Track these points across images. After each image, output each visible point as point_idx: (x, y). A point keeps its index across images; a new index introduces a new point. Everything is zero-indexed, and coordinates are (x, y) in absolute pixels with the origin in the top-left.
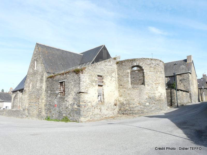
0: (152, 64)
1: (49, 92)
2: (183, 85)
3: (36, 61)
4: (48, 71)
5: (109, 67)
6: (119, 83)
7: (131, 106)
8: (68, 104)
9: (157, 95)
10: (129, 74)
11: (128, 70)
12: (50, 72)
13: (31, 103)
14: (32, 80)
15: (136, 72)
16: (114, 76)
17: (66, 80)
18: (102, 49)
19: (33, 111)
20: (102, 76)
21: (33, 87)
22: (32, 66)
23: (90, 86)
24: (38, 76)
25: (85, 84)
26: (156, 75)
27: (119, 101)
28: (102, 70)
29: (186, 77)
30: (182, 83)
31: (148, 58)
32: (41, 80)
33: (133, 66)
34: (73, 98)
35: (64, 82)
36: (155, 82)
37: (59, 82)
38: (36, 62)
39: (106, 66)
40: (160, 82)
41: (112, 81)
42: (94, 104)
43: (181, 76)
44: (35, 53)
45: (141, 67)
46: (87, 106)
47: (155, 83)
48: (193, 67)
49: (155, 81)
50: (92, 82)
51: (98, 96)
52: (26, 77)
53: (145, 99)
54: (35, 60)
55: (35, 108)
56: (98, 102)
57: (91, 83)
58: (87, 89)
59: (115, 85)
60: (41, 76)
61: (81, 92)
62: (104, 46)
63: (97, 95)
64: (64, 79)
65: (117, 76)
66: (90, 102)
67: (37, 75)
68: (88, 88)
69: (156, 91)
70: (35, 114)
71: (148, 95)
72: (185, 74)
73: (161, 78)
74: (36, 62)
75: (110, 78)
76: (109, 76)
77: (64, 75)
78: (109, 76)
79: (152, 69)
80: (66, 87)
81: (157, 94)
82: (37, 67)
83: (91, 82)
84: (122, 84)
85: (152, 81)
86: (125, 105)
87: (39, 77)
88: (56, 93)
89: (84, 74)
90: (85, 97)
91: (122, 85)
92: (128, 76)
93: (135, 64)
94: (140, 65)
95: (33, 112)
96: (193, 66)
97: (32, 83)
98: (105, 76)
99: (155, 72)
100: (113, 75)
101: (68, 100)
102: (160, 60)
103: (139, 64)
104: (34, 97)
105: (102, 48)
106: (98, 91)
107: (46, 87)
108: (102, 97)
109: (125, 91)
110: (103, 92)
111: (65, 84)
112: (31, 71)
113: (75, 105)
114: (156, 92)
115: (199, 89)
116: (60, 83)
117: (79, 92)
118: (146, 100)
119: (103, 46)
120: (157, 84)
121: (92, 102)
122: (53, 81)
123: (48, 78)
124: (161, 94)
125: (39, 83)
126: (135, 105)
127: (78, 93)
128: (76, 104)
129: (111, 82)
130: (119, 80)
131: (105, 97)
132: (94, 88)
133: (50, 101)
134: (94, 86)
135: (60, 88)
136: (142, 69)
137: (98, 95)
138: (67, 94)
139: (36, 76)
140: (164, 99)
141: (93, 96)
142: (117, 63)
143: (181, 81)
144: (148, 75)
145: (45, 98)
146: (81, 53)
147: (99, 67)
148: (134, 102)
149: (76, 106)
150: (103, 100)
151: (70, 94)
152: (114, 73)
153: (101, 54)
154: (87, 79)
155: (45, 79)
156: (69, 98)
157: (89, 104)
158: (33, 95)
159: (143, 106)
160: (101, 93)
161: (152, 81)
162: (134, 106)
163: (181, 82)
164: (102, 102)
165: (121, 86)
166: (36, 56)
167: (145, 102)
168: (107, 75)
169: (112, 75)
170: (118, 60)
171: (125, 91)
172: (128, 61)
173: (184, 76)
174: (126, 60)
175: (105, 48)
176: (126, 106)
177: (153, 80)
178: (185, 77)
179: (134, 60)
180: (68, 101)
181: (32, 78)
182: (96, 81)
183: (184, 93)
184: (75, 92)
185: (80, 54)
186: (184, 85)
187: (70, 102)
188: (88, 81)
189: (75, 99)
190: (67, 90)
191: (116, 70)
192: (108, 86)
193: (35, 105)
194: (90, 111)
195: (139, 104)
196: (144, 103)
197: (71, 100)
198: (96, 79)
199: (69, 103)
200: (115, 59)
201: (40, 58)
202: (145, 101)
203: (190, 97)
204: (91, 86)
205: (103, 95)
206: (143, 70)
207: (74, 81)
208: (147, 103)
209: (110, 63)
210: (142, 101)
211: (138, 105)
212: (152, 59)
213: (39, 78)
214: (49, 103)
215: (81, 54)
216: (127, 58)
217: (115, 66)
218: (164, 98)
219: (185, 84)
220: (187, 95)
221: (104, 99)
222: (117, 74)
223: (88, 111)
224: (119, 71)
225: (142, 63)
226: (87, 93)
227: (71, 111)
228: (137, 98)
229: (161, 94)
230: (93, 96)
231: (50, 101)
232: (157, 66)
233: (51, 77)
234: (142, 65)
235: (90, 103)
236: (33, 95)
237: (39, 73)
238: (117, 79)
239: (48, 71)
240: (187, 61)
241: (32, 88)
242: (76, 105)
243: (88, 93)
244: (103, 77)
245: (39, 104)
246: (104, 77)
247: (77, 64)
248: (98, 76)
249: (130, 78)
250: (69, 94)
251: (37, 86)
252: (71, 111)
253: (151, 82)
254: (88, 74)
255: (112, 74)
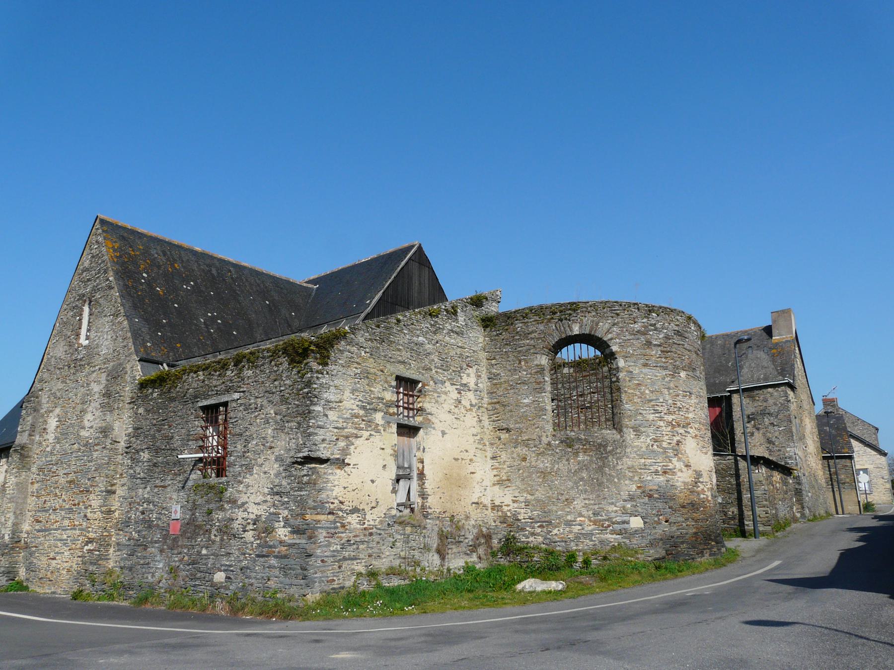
0: (656, 329)
1: (145, 456)
2: (763, 440)
3: (89, 304)
4: (148, 354)
5: (447, 338)
6: (494, 418)
7: (555, 531)
8: (240, 521)
9: (682, 478)
10: (547, 373)
11: (538, 356)
12: (154, 355)
13: (47, 511)
14: (58, 394)
15: (566, 370)
16: (472, 385)
17: (236, 396)
18: (407, 263)
19: (52, 555)
20: (416, 382)
21: (63, 434)
22: (66, 328)
23: (356, 428)
24: (94, 375)
25: (333, 416)
26: (672, 385)
27: (493, 509)
28: (416, 349)
29: (775, 404)
30: (758, 429)
31: (635, 304)
32: (107, 394)
33: (564, 336)
34: (266, 491)
35: (225, 404)
36: (670, 418)
37: (200, 404)
38: (86, 309)
39: (435, 333)
40: (691, 416)
41: (463, 410)
42: (373, 518)
43: (753, 398)
44: (87, 264)
45: (605, 342)
46: (341, 530)
47: (670, 423)
48: (799, 361)
49: (670, 413)
50: (369, 408)
51: (398, 481)
52: (20, 406)
53: (625, 501)
54: (81, 298)
55: (65, 537)
56: (394, 512)
57: (362, 412)
58: (342, 444)
59: (477, 430)
60: (108, 375)
61: (313, 455)
62: (420, 248)
63: (392, 472)
64: (228, 390)
65: (484, 384)
66: (355, 510)
67: (87, 369)
68: (347, 437)
69: (674, 460)
70: (64, 572)
71: (636, 478)
72: (770, 390)
73: (693, 397)
74: (86, 309)
75: (455, 395)
76: (448, 384)
77: (229, 373)
78: (448, 384)
79: (655, 352)
80: (237, 430)
81: (679, 474)
82: (88, 330)
83: (364, 408)
84: (512, 426)
85: (656, 412)
86: (523, 529)
87: (99, 382)
88: (179, 462)
89: (334, 367)
90: (338, 485)
91: (508, 430)
92: (539, 383)
93: (576, 330)
94: (602, 330)
95: (54, 559)
96: (798, 356)
97: (58, 411)
98: (431, 383)
99: (665, 368)
100: (470, 378)
101: (243, 498)
102: (688, 312)
103: (592, 328)
104: (62, 480)
105: (408, 257)
106: (396, 455)
107: (130, 430)
108: (415, 484)
109: (524, 459)
110: (422, 462)
111: (232, 414)
112: (60, 351)
113: (277, 525)
114: (676, 464)
115: (824, 458)
116: (205, 409)
117: (305, 458)
118: (629, 506)
119: (413, 246)
120: (679, 425)
121: (367, 509)
122: (172, 400)
123: (143, 385)
124: (698, 474)
125: (98, 413)
126: (576, 529)
127: (296, 463)
128: (286, 520)
129: (456, 410)
130: (497, 406)
131: (429, 485)
132: (377, 440)
133: (149, 502)
134: (378, 431)
135: (204, 438)
136: (607, 351)
137: (394, 477)
138: (237, 469)
139: (81, 376)
140: (709, 501)
141: (373, 481)
142: (487, 322)
143: (753, 419)
144: (639, 384)
145: (123, 485)
146: (306, 280)
147: (404, 338)
148: (569, 513)
149: (282, 532)
150: (419, 500)
151: (256, 469)
152: (472, 371)
153: (402, 286)
154: (347, 394)
155: (128, 391)
156: (248, 486)
157: (353, 520)
158: (61, 473)
159: (613, 532)
160: (410, 468)
161: (656, 412)
162: (571, 532)
163: (754, 426)
164: (412, 510)
165: (504, 436)
166: (89, 280)
167: (625, 512)
168: (440, 378)
169: (464, 382)
170: (492, 309)
171: (524, 459)
172: (540, 312)
173: (766, 400)
174: (531, 309)
175: (420, 257)
176: (533, 534)
177: (660, 409)
178: (771, 401)
179: (572, 309)
180: (243, 504)
181: (60, 385)
182: (389, 405)
183: (777, 476)
184: (279, 459)
185: (305, 285)
186: (769, 441)
187: (254, 510)
188: (350, 404)
189: (277, 494)
190: (239, 447)
191: (483, 355)
192: (444, 433)
193: (66, 522)
194: (355, 558)
195: (595, 522)
196: (619, 519)
197: (260, 498)
198: (389, 396)
199: (245, 515)
200: (477, 302)
201: (111, 288)
202: (624, 507)
203: (798, 493)
204: (362, 429)
205: (421, 475)
206: (612, 356)
207: (276, 398)
208: (632, 519)
209: (457, 320)
210: (612, 508)
211: (589, 528)
212: (651, 309)
213: (96, 388)
214: (143, 513)
215: (309, 282)
216: (535, 303)
217: (478, 337)
218: (709, 494)
219: (775, 433)
220: (785, 483)
221: (423, 495)
222: (484, 376)
223: (345, 559)
224: (493, 362)
225: (607, 326)
226: (341, 463)
227: (258, 556)
228: (586, 491)
229: (698, 474)
230: (373, 481)
231: (149, 502)
232: (677, 340)
233: (159, 381)
234: (610, 336)
235: (355, 516)
236: (61, 473)
237: (98, 360)
238: (486, 400)
239: (148, 354)
240: (775, 332)
241: (56, 438)
242: (282, 524)
243: (346, 461)
244: (420, 385)
245: (89, 515)
246: (424, 386)
247: (289, 326)
248: (399, 379)
249: (550, 396)
250: (249, 468)
251: (87, 424)
252: (258, 556)
253: (651, 417)
254: (353, 370)
255: (465, 376)
